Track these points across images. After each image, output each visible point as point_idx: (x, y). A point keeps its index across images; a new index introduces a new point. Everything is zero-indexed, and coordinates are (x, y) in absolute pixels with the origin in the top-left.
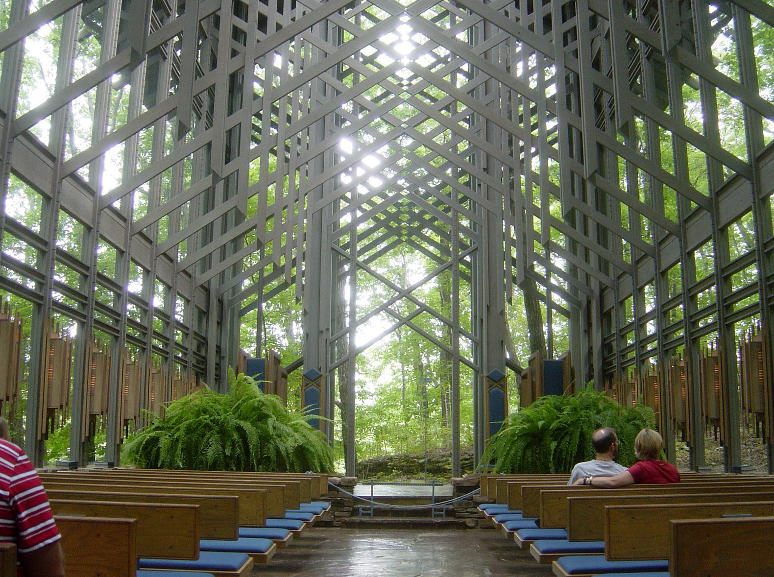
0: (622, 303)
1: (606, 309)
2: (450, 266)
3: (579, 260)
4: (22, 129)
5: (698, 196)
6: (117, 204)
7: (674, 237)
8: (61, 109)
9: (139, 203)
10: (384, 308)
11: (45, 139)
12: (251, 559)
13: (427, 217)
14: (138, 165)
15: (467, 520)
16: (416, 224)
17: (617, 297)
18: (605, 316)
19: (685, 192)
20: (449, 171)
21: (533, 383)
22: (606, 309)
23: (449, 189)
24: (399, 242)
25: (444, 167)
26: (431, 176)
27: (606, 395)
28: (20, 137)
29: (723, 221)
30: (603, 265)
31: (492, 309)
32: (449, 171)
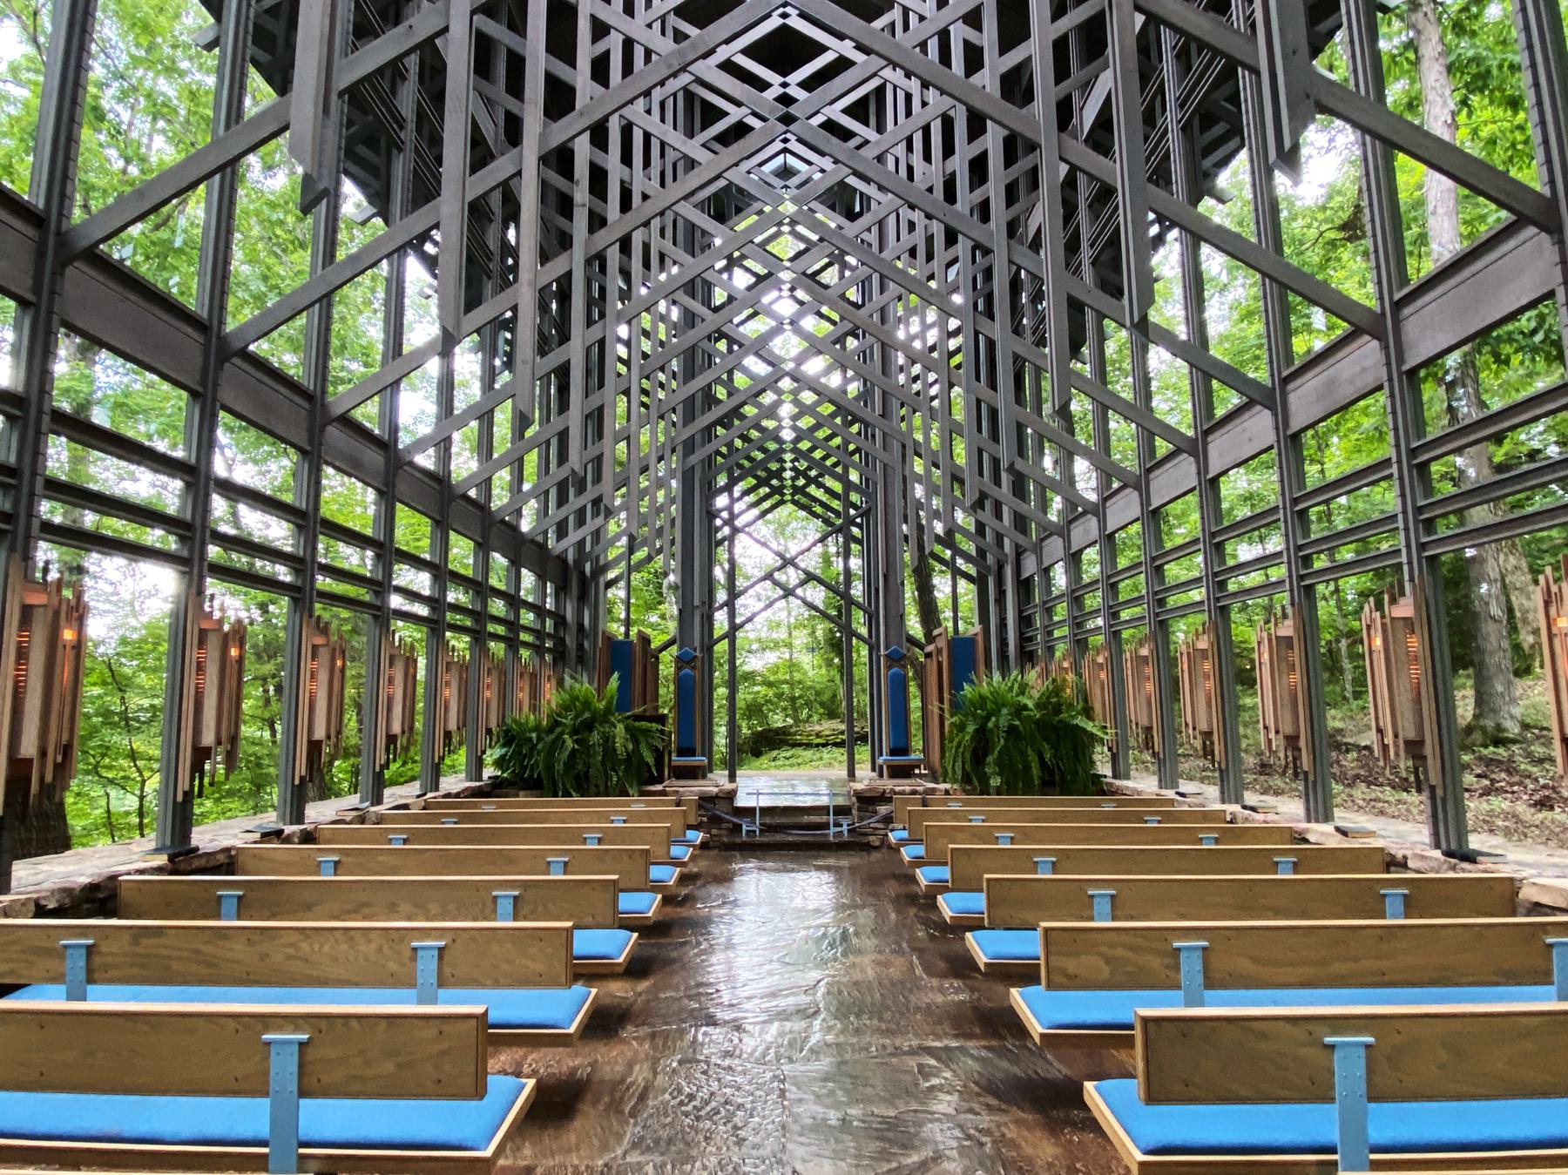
0: (1047, 570)
1: (1025, 575)
2: (839, 530)
3: (987, 516)
4: (240, 345)
5: (1169, 432)
6: (472, 493)
7: (1129, 490)
8: (88, 136)
9: (104, 843)
10: (769, 576)
11: (289, 361)
12: (635, 935)
13: (813, 473)
14: (1131, 631)
15: (871, 838)
16: (801, 482)
17: (1040, 560)
18: (1024, 586)
19: (1149, 428)
20: (838, 420)
21: (940, 665)
22: (1025, 575)
23: (837, 441)
24: (782, 502)
25: (833, 416)
26: (817, 426)
27: (1088, 713)
28: (236, 360)
29: (1214, 470)
30: (1021, 523)
31: (891, 579)
32: (838, 420)
